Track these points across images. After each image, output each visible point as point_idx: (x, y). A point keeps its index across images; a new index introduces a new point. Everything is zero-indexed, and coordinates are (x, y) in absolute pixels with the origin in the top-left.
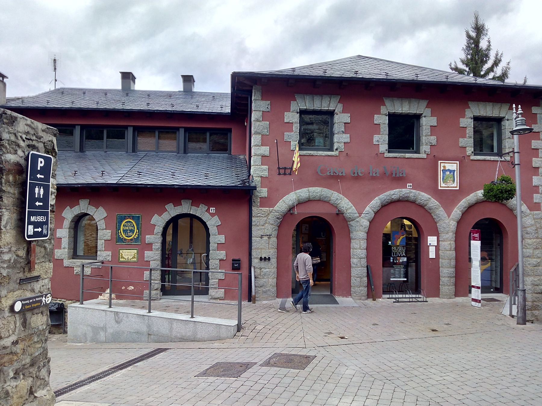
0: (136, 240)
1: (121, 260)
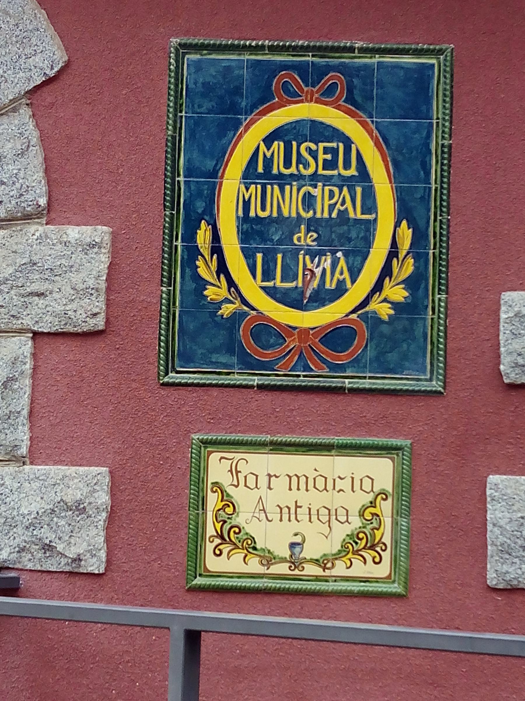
0: (393, 339)
1: (224, 564)
